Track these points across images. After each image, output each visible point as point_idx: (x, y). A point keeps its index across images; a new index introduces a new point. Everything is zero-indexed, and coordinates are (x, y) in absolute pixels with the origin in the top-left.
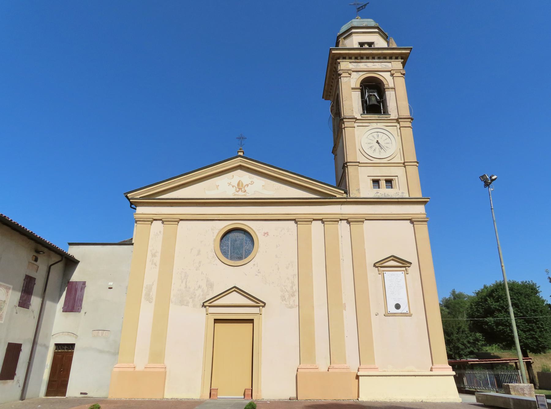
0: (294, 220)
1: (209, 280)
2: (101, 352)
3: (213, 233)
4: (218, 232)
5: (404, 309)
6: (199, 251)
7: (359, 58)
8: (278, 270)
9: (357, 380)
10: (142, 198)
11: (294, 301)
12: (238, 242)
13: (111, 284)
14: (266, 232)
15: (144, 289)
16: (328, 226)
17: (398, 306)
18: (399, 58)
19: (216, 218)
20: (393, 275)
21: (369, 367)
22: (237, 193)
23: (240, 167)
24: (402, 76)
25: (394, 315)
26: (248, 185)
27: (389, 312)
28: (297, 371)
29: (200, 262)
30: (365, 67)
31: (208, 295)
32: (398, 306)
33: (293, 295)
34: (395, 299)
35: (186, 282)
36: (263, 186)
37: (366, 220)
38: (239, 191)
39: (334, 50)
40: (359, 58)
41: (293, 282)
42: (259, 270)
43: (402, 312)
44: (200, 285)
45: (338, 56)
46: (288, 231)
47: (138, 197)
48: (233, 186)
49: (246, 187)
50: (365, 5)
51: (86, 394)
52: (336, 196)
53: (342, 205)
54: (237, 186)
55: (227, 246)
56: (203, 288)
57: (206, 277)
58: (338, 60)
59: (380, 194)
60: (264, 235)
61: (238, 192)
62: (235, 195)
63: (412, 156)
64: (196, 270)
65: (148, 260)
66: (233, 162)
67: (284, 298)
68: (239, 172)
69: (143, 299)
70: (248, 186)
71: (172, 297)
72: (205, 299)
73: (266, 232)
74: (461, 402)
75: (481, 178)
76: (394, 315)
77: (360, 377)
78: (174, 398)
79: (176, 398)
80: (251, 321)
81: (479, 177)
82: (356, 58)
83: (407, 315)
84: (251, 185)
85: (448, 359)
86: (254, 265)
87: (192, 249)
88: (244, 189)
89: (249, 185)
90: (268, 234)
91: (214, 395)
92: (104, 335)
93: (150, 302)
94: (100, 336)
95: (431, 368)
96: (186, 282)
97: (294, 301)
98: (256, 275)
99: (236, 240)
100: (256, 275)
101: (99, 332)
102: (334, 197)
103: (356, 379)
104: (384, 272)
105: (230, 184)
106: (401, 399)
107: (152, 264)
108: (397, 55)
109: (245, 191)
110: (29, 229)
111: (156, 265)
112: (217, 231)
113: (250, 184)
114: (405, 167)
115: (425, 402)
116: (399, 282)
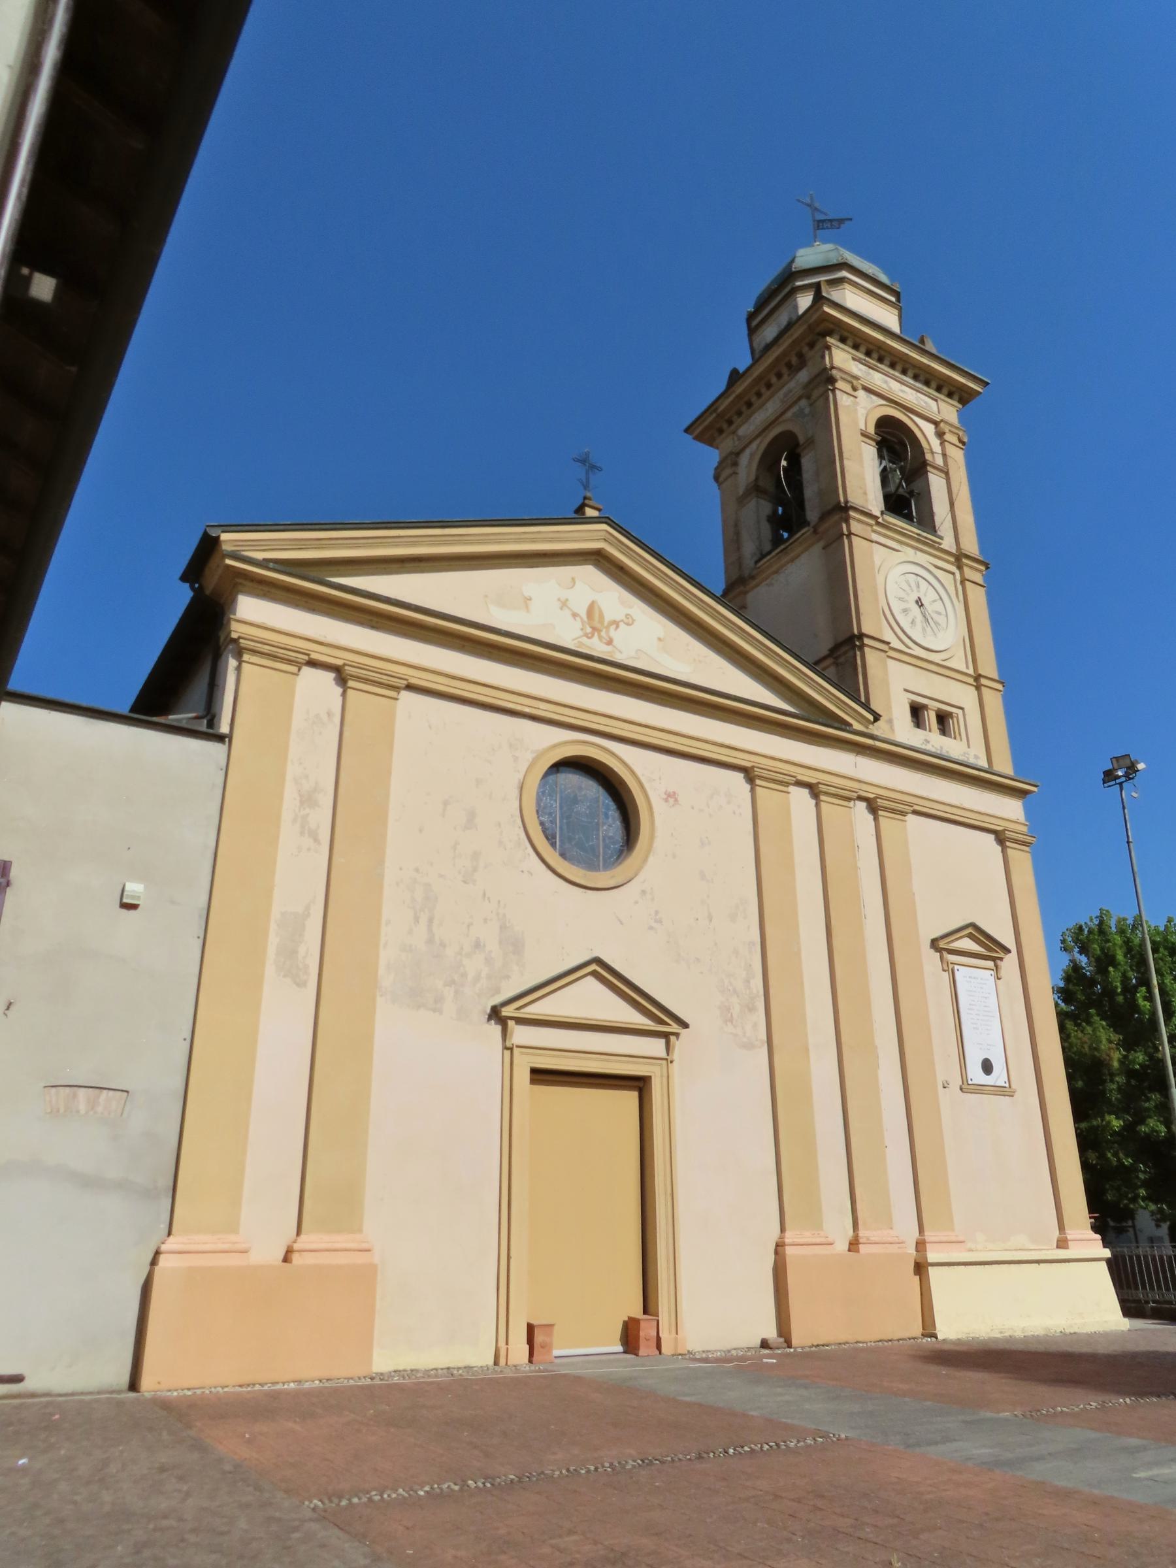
0: (745, 770)
1: (508, 925)
2: (91, 1183)
3: (516, 759)
4: (531, 760)
5: (998, 1077)
6: (471, 816)
7: (875, 355)
8: (711, 921)
9: (918, 1277)
10: (277, 566)
11: (755, 1025)
12: (581, 808)
13: (135, 889)
14: (672, 791)
15: (273, 926)
16: (830, 808)
17: (987, 1067)
18: (956, 397)
19: (527, 710)
20: (975, 978)
21: (944, 1239)
22: (585, 640)
23: (598, 558)
24: (960, 445)
25: (980, 1089)
26: (616, 624)
27: (971, 1080)
28: (154, 1262)
29: (476, 856)
30: (884, 386)
31: (508, 977)
32: (987, 1067)
33: (752, 1009)
34: (982, 1044)
35: (431, 921)
36: (660, 639)
37: (916, 812)
38: (593, 635)
39: (829, 307)
40: (875, 355)
41: (750, 965)
42: (657, 912)
43: (997, 1084)
44: (478, 938)
45: (831, 326)
46: (729, 803)
47: (260, 556)
48: (575, 615)
49: (612, 628)
50: (841, 221)
51: (17, 1379)
52: (850, 725)
53: (858, 753)
54: (585, 618)
55: (550, 814)
56: (491, 952)
57: (498, 914)
58: (828, 339)
59: (933, 746)
60: (666, 800)
61: (589, 638)
62: (581, 644)
63: (989, 666)
64: (465, 882)
65: (287, 815)
66: (576, 535)
67: (730, 1015)
68: (589, 573)
69: (270, 971)
70: (617, 627)
71: (382, 971)
72: (497, 991)
73: (671, 790)
74: (1129, 1330)
75: (1114, 760)
76: (980, 1089)
77: (929, 1268)
78: (405, 1371)
79: (408, 1368)
80: (640, 1084)
81: (1111, 759)
82: (868, 354)
83: (1005, 1091)
84: (627, 626)
85: (1089, 1213)
86: (644, 892)
87: (446, 803)
88: (607, 632)
89: (622, 625)
90: (676, 800)
91: (542, 1347)
92: (100, 1109)
93: (298, 985)
94: (83, 1112)
95: (777, 1245)
96: (431, 921)
97: (755, 1025)
98: (651, 928)
99: (575, 801)
100: (651, 928)
101: (75, 1096)
102: (844, 725)
103: (915, 1275)
104: (956, 967)
105: (564, 604)
106: (1023, 1329)
107: (302, 833)
108: (954, 386)
109: (610, 642)
110: (947, 495)
111: (316, 840)
112: (529, 756)
113: (622, 621)
114: (978, 688)
115: (1071, 1334)
116: (986, 998)
